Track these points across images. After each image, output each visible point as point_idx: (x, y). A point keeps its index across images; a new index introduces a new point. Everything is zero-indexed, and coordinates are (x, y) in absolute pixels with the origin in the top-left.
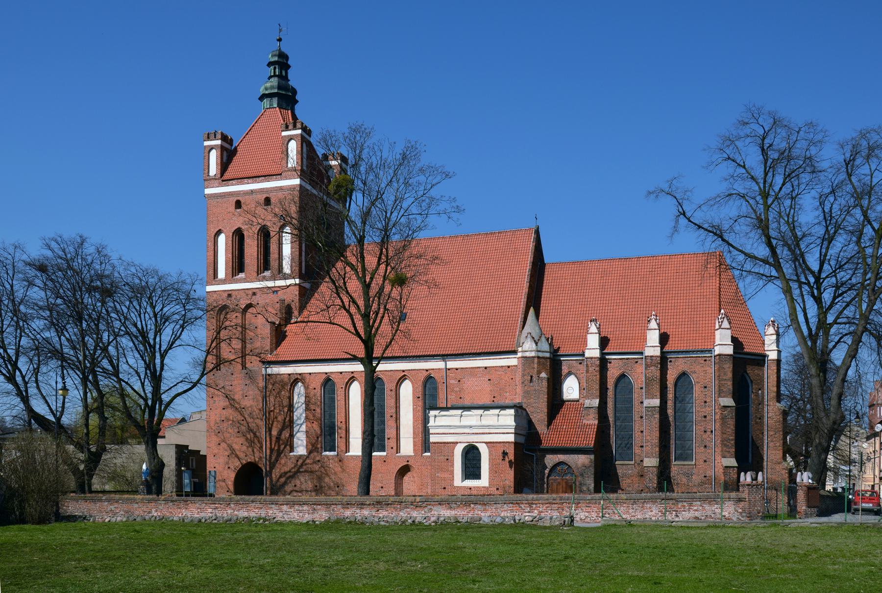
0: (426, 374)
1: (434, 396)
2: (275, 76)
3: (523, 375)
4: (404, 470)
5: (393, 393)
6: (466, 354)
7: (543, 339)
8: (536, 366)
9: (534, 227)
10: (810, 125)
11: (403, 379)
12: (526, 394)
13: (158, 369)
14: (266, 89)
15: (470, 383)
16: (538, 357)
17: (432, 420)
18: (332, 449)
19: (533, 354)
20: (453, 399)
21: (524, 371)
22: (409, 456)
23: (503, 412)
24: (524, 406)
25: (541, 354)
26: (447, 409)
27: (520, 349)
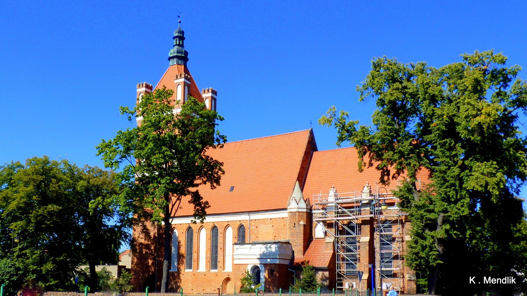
0: (239, 223)
1: (244, 237)
2: (176, 45)
3: (290, 223)
4: (228, 279)
5: (222, 235)
6: (261, 211)
7: (302, 200)
8: (297, 217)
9: (310, 129)
10: (222, 147)
11: (228, 226)
12: (292, 235)
13: (170, 211)
14: (171, 54)
15: (263, 228)
16: (299, 212)
17: (235, 250)
18: (190, 268)
19: (296, 210)
20: (253, 239)
21: (291, 220)
22: (229, 272)
23: (254, 246)
24: (290, 242)
25: (300, 210)
26: (254, 244)
27: (289, 207)
